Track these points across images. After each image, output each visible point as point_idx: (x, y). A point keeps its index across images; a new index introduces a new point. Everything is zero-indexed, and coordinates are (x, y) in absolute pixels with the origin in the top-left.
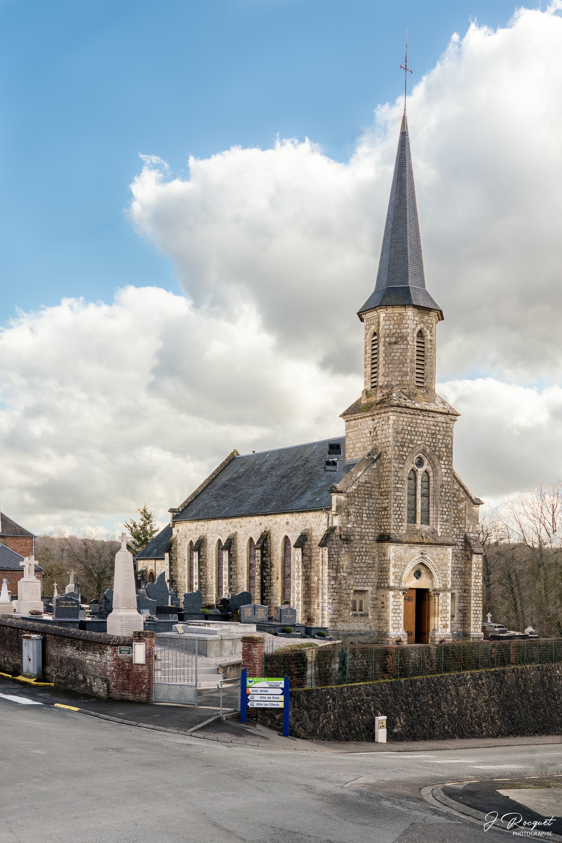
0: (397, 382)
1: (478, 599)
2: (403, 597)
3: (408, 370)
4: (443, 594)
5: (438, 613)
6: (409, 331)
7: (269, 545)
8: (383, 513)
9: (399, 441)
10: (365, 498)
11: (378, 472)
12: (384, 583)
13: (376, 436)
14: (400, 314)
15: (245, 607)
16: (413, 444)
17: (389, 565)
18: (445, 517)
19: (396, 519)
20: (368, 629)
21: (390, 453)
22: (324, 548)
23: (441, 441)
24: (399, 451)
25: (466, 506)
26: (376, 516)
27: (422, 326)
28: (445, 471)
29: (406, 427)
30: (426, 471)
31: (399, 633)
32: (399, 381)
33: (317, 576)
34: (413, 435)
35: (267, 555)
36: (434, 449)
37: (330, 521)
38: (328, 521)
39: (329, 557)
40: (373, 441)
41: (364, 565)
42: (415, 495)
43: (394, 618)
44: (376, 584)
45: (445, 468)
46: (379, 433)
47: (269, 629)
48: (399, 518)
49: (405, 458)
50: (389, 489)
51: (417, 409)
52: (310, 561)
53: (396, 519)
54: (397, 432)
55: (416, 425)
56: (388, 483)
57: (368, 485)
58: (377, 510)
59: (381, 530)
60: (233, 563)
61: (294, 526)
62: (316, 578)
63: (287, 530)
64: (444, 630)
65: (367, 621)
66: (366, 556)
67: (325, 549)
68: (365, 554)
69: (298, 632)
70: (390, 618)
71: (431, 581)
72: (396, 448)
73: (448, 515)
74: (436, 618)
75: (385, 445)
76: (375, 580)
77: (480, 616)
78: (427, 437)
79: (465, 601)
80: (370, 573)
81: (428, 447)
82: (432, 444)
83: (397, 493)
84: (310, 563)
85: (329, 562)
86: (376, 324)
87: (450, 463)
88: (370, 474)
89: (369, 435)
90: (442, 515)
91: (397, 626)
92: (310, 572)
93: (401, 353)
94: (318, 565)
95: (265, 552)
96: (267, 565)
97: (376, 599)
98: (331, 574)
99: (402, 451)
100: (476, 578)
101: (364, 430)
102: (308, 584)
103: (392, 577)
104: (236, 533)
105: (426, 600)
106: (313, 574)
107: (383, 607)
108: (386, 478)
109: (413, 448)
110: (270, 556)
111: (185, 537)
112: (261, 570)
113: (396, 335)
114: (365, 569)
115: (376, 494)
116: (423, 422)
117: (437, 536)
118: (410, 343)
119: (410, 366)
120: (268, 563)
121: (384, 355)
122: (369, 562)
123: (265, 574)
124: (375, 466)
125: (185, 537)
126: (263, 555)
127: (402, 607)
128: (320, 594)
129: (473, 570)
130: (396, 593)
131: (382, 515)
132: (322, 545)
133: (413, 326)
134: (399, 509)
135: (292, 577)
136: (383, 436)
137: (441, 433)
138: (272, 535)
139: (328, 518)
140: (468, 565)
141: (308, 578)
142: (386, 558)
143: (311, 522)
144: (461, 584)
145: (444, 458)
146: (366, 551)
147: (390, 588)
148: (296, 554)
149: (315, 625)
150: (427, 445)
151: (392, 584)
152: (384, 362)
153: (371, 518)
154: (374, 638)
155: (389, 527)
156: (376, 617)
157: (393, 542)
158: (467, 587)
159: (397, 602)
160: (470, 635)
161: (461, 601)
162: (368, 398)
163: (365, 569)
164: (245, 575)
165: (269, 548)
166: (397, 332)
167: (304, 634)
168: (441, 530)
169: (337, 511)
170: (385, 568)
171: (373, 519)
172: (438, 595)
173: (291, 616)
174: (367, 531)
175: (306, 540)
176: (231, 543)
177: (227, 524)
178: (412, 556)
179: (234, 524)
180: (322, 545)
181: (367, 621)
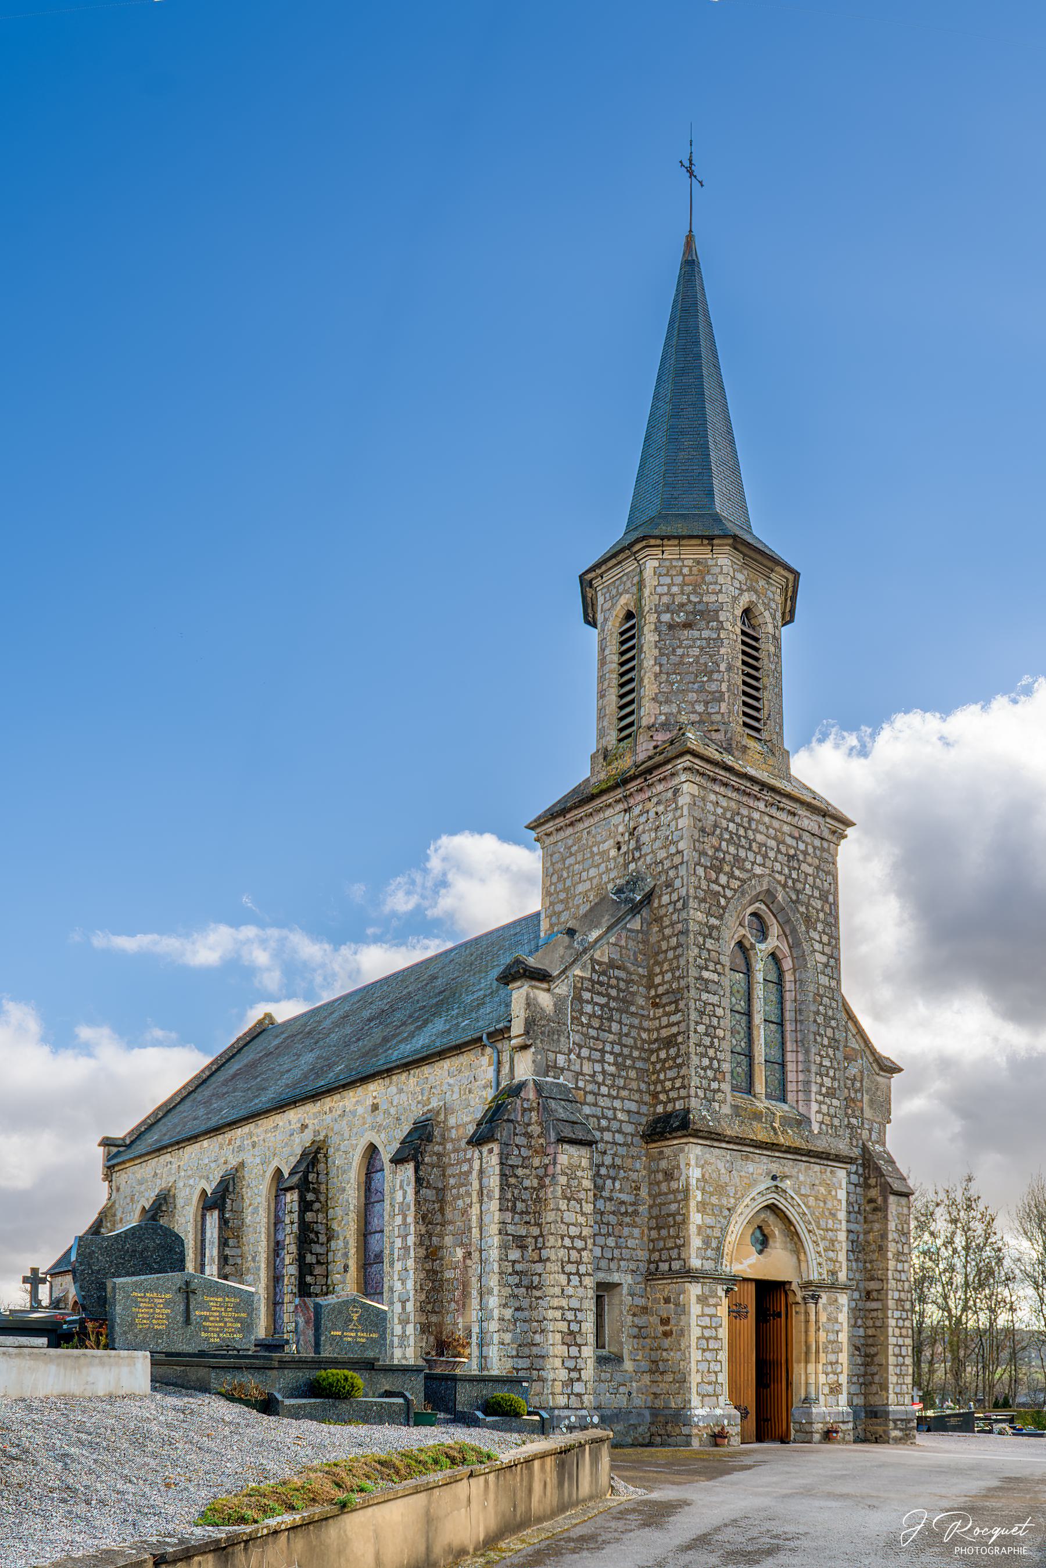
0: (695, 717)
1: (904, 1314)
2: (725, 1302)
3: (724, 689)
4: (829, 1298)
5: (817, 1352)
6: (722, 598)
7: (322, 1178)
8: (663, 1055)
9: (706, 854)
10: (611, 1009)
11: (645, 942)
12: (670, 1260)
13: (638, 848)
14: (698, 562)
15: (137, 1286)
16: (742, 869)
17: (687, 1206)
18: (827, 1082)
19: (705, 1069)
20: (621, 1401)
21: (688, 881)
22: (485, 1149)
23: (810, 879)
24: (709, 881)
25: (862, 1072)
26: (639, 1064)
28: (824, 959)
29: (724, 823)
30: (773, 955)
31: (719, 1412)
32: (700, 714)
33: (462, 1245)
34: (743, 847)
35: (317, 1206)
36: (794, 897)
37: (505, 1069)
38: (498, 1072)
39: (503, 1175)
40: (626, 865)
41: (610, 1207)
42: (749, 1014)
43: (704, 1366)
44: (643, 1267)
45: (823, 953)
46: (645, 838)
47: (228, 1381)
48: (710, 1067)
50: (683, 983)
51: (752, 780)
52: (442, 1201)
53: (705, 1069)
54: (702, 830)
55: (749, 822)
56: (678, 968)
57: (617, 973)
58: (642, 1049)
59: (655, 1106)
60: (231, 1242)
61: (393, 1111)
62: (460, 1253)
63: (373, 1128)
64: (831, 1399)
65: (618, 1377)
66: (614, 1179)
67: (491, 1151)
68: (612, 1173)
69: (388, 1394)
70: (693, 1365)
71: (795, 1259)
72: (700, 871)
73: (834, 1079)
74: (811, 1367)
75: (667, 864)
76: (640, 1253)
77: (909, 1361)
78: (776, 860)
79: (870, 1323)
80: (626, 1231)
81: (779, 888)
82: (790, 883)
83: (705, 996)
84: (442, 1210)
85: (502, 1190)
86: (635, 589)
87: (834, 942)
88: (623, 943)
89: (613, 853)
90: (821, 1076)
91: (710, 1389)
92: (441, 1236)
93: (702, 648)
94: (464, 1212)
95: (310, 1197)
96: (317, 1233)
97: (645, 1310)
98: (510, 1229)
99: (716, 882)
100: (898, 1261)
101: (598, 844)
102: (435, 1272)
103: (696, 1242)
104: (242, 1164)
105: (779, 1315)
106: (448, 1240)
107: (666, 1334)
108: (670, 954)
109: (743, 881)
110: (325, 1209)
111: (132, 1200)
112: (300, 1248)
113: (690, 608)
114: (613, 1219)
115: (641, 1001)
116: (767, 819)
117: (811, 1131)
118: (727, 625)
119: (729, 680)
120: (321, 1229)
121: (656, 652)
122: (624, 1197)
123: (310, 1259)
124: (636, 924)
125: (132, 1200)
126: (305, 1206)
127: (723, 1333)
128: (475, 1293)
129: (890, 1238)
130: (706, 1288)
131: (659, 1060)
132: (478, 1141)
134: (712, 1043)
135: (386, 1260)
136: (658, 844)
137: (809, 859)
138: (331, 1151)
139: (499, 1063)
140: (877, 1226)
141: (434, 1253)
142: (674, 1185)
143: (445, 1087)
144: (858, 1276)
145: (820, 927)
146: (613, 1166)
147: (689, 1275)
148: (399, 1185)
149: (469, 1364)
150: (779, 882)
151: (695, 1263)
152: (657, 668)
153: (627, 1068)
154: (640, 1430)
155: (683, 1093)
156: (645, 1365)
157: (696, 1134)
158: (873, 1285)
159: (711, 1316)
160: (887, 1413)
161: (860, 1322)
162: (609, 764)
163: (613, 1219)
164: (263, 1274)
165: (323, 1187)
166: (690, 601)
167: (417, 1398)
168: (819, 1117)
169: (527, 1033)
170: (673, 1215)
171: (633, 1074)
172: (816, 1298)
173: (363, 1337)
174: (617, 1104)
175: (429, 1139)
176: (227, 1189)
177: (221, 1148)
178: (751, 1181)
179: (238, 1143)
180: (478, 1141)
181: (618, 1377)
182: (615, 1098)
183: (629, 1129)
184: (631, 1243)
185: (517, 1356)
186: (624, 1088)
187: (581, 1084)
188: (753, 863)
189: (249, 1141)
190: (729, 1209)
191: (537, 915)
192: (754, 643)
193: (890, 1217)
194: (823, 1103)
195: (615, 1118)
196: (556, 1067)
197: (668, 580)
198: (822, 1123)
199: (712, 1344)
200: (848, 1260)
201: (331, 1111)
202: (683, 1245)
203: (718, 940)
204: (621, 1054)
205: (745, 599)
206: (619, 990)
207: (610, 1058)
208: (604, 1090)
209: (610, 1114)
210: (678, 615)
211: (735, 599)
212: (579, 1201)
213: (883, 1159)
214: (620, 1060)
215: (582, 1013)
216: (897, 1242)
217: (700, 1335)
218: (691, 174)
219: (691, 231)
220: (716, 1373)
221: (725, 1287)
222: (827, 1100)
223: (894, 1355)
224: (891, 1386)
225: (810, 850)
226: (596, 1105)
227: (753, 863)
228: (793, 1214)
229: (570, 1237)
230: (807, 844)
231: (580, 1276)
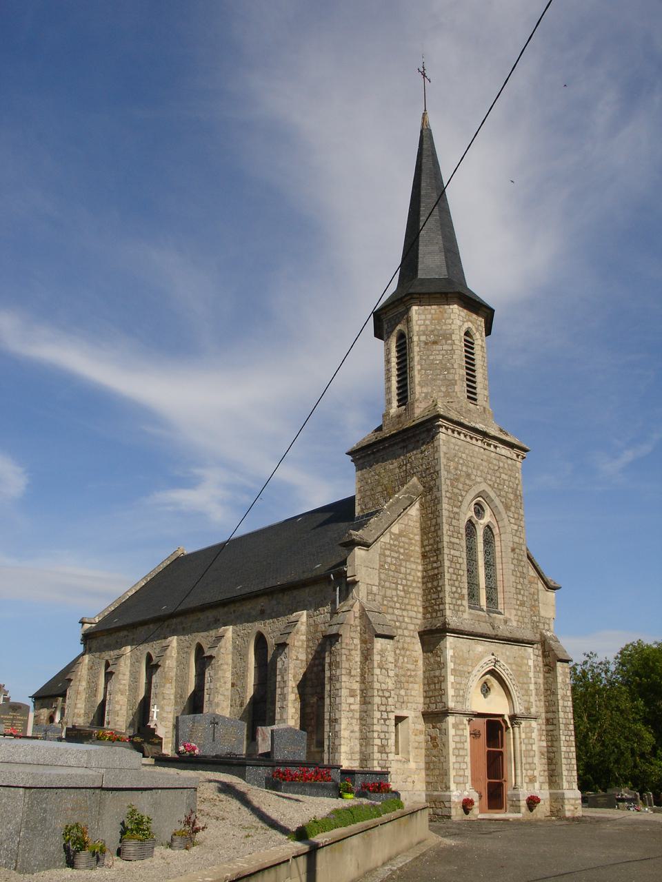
1: (569, 732)
2: (468, 728)
19: (453, 593)
27: (470, 325)
30: (488, 526)
43: (457, 766)
49: (460, 498)
53: (453, 593)
66: (404, 656)
68: (403, 652)
70: (451, 765)
82: (496, 485)
83: (452, 552)
93: (443, 355)
103: (451, 692)
118: (456, 342)
122: (409, 666)
127: (468, 746)
133: (459, 323)
137: (506, 471)
145: (513, 509)
153: (410, 593)
159: (460, 736)
166: (435, 329)
174: (405, 613)
179: (173, 627)
182: (404, 610)
183: (412, 627)
184: (413, 693)
185: (351, 759)
186: (408, 604)
187: (385, 602)
188: (476, 476)
189: (181, 627)
190: (469, 673)
191: (353, 498)
192: (471, 362)
193: (558, 675)
194: (518, 610)
195: (404, 621)
196: (371, 593)
197: (423, 317)
198: (518, 621)
199: (462, 753)
200: (536, 701)
201: (234, 611)
202: (444, 694)
203: (458, 520)
204: (406, 585)
205: (466, 325)
206: (405, 549)
207: (400, 587)
208: (398, 605)
209: (401, 619)
210: (430, 337)
211: (460, 327)
212: (387, 670)
213: (553, 640)
214: (406, 588)
215: (385, 562)
216: (563, 689)
217: (454, 747)
218: (424, 75)
219: (425, 110)
220: (464, 769)
221: (468, 718)
222: (521, 608)
223: (565, 758)
224: (564, 777)
225: (506, 466)
226: (393, 614)
227: (476, 476)
228: (505, 677)
229: (382, 690)
230: (504, 463)
231: (387, 712)
